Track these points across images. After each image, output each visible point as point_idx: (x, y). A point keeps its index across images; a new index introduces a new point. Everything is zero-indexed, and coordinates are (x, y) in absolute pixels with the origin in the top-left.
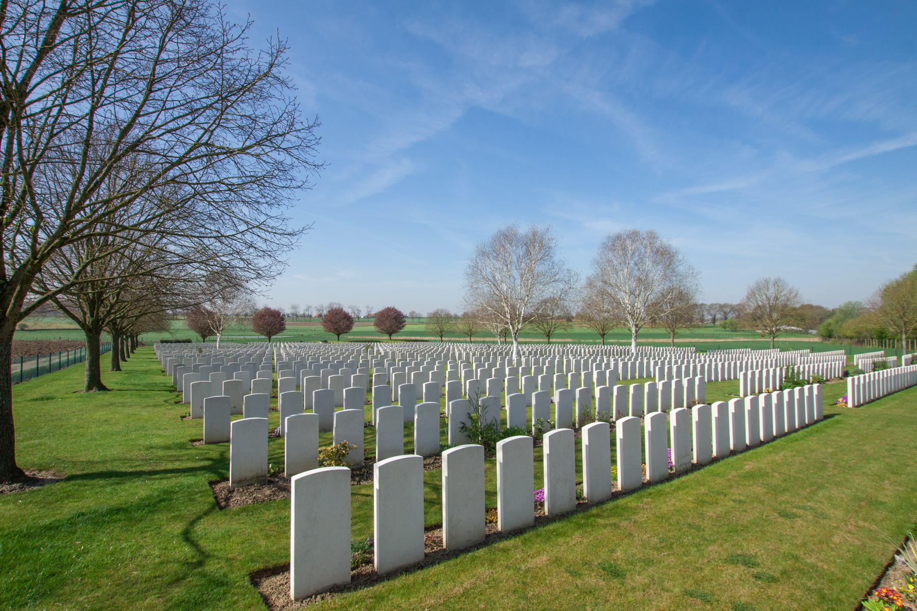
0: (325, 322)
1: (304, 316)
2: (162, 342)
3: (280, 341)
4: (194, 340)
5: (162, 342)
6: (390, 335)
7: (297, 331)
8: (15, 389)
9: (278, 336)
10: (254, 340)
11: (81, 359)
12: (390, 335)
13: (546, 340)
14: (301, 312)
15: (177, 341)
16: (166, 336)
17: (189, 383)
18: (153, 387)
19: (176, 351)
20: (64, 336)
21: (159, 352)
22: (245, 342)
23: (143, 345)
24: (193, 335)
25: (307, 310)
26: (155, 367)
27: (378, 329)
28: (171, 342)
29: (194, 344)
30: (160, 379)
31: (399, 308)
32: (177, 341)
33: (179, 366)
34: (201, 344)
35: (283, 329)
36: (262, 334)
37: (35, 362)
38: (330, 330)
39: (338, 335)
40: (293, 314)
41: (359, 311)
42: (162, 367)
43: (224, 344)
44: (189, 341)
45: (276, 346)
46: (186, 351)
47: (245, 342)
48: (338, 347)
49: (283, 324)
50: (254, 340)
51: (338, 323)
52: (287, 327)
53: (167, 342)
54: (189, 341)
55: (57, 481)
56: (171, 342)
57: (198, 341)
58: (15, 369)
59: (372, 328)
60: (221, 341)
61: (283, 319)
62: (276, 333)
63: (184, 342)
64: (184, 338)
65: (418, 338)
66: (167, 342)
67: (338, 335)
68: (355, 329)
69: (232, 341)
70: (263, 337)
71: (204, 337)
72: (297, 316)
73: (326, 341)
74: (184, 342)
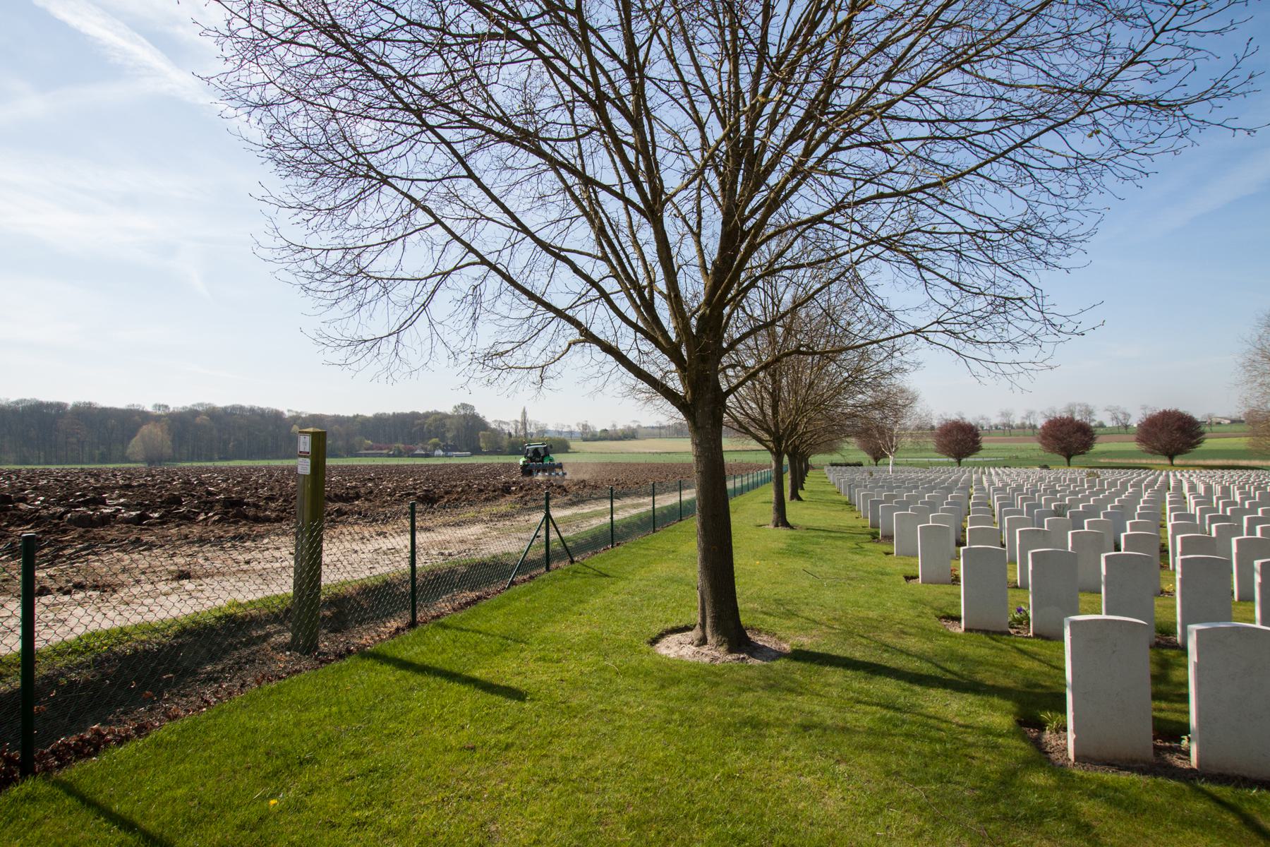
0: (1044, 437)
1: (1023, 427)
2: (832, 465)
3: (974, 464)
4: (865, 462)
5: (832, 465)
6: (1171, 458)
7: (1010, 450)
8: (733, 503)
9: (970, 459)
10: (939, 464)
11: (679, 513)
12: (1171, 458)
13: (1168, 462)
14: (1017, 421)
15: (848, 465)
16: (836, 458)
17: (859, 495)
18: (834, 502)
19: (848, 473)
20: (746, 458)
21: (832, 475)
22: (925, 466)
23: (813, 468)
24: (864, 457)
25: (1028, 417)
26: (829, 489)
27: (1144, 448)
28: (841, 465)
29: (865, 468)
30: (837, 497)
31: (1184, 408)
32: (848, 465)
33: (851, 485)
34: (873, 468)
35: (979, 449)
36: (949, 456)
37: (46, 638)
38: (1053, 451)
39: (1069, 457)
40: (1004, 425)
41: (1127, 416)
42: (836, 489)
43: (900, 468)
44: (860, 465)
45: (984, 473)
46: (858, 474)
47: (925, 466)
48: (1069, 475)
49: (978, 442)
50: (939, 464)
51: (1070, 438)
52: (984, 445)
53: (836, 465)
54: (860, 465)
55: (994, 81)
56: (841, 465)
57: (870, 464)
58: (730, 485)
59: (1133, 446)
60: (895, 464)
61: (977, 435)
62: (967, 455)
63: (855, 465)
64: (855, 462)
65: (1236, 462)
66: (836, 465)
67: (1069, 457)
68: (1098, 447)
69: (911, 465)
70: (951, 460)
71: (876, 459)
72: (1011, 427)
73: (1046, 467)
74: (855, 465)
